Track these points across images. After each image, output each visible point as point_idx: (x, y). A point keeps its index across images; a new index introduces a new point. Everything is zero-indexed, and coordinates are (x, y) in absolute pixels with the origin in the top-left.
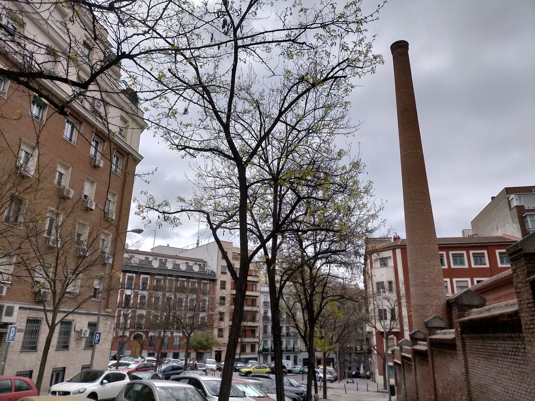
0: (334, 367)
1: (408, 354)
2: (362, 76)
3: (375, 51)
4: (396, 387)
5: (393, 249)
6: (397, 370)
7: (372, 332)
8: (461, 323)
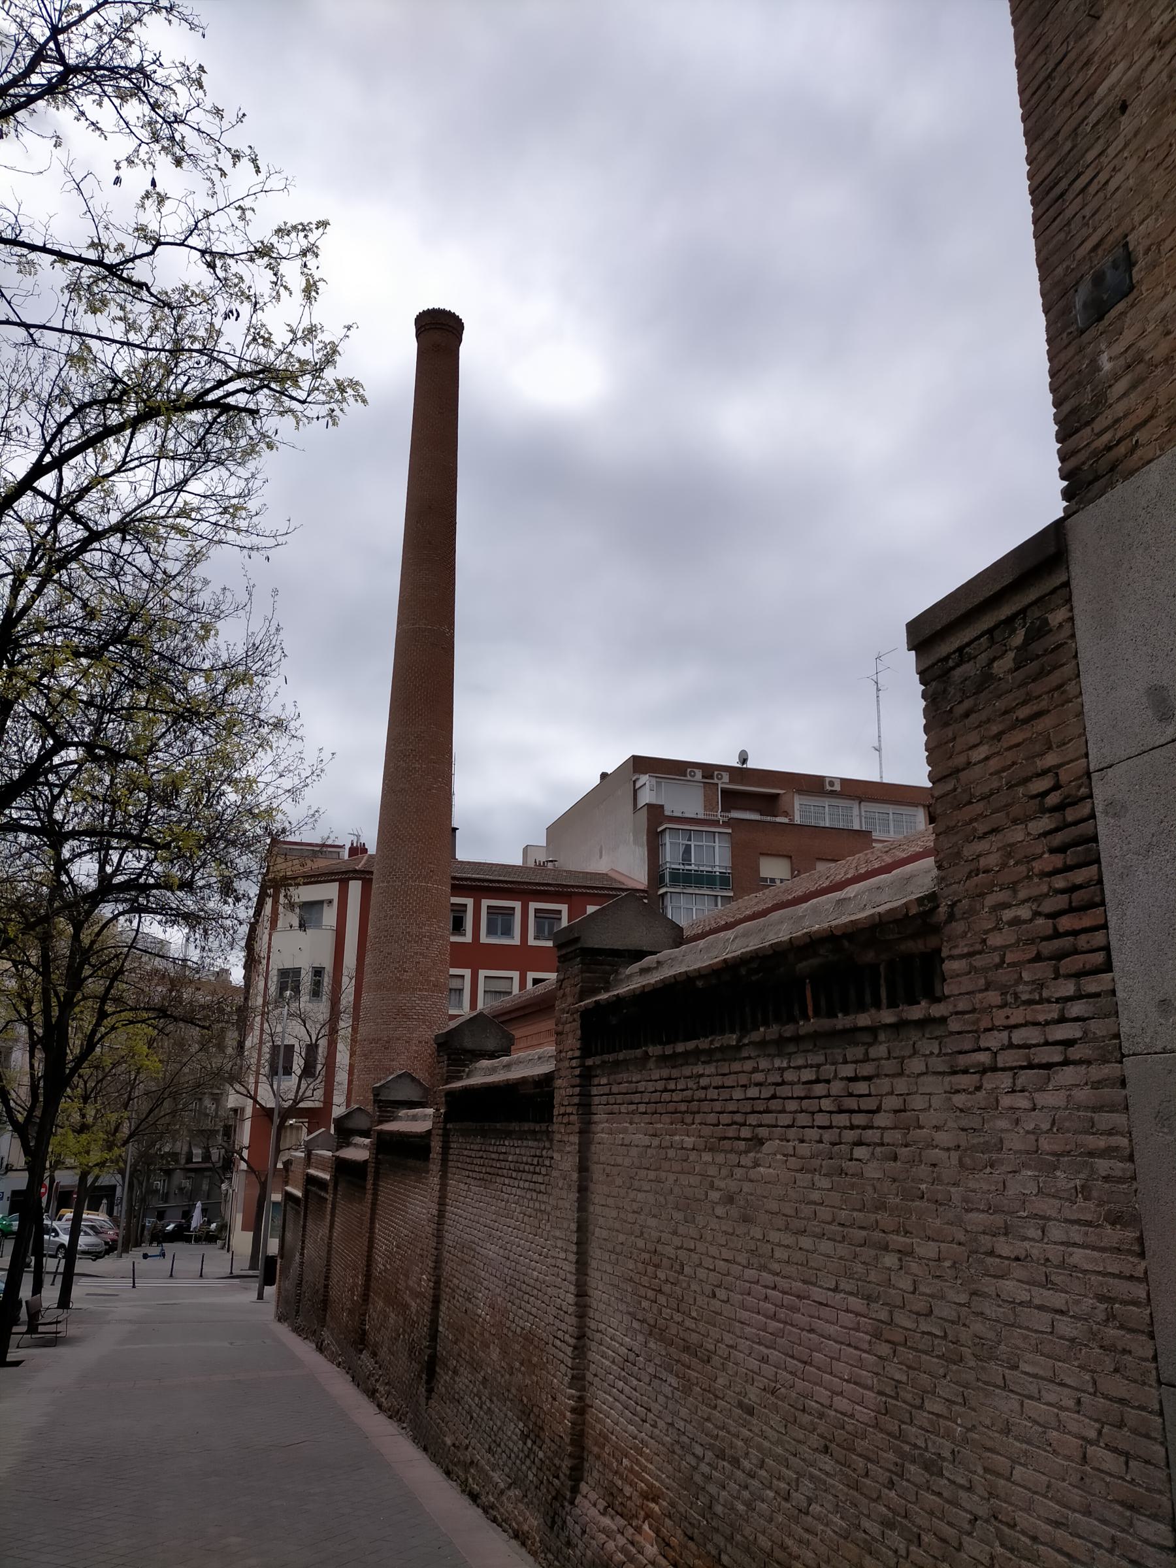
0: (110, 1213)
1: (323, 1170)
4: (279, 1261)
5: (342, 878)
6: (290, 1215)
7: (243, 1109)
8: (450, 1094)
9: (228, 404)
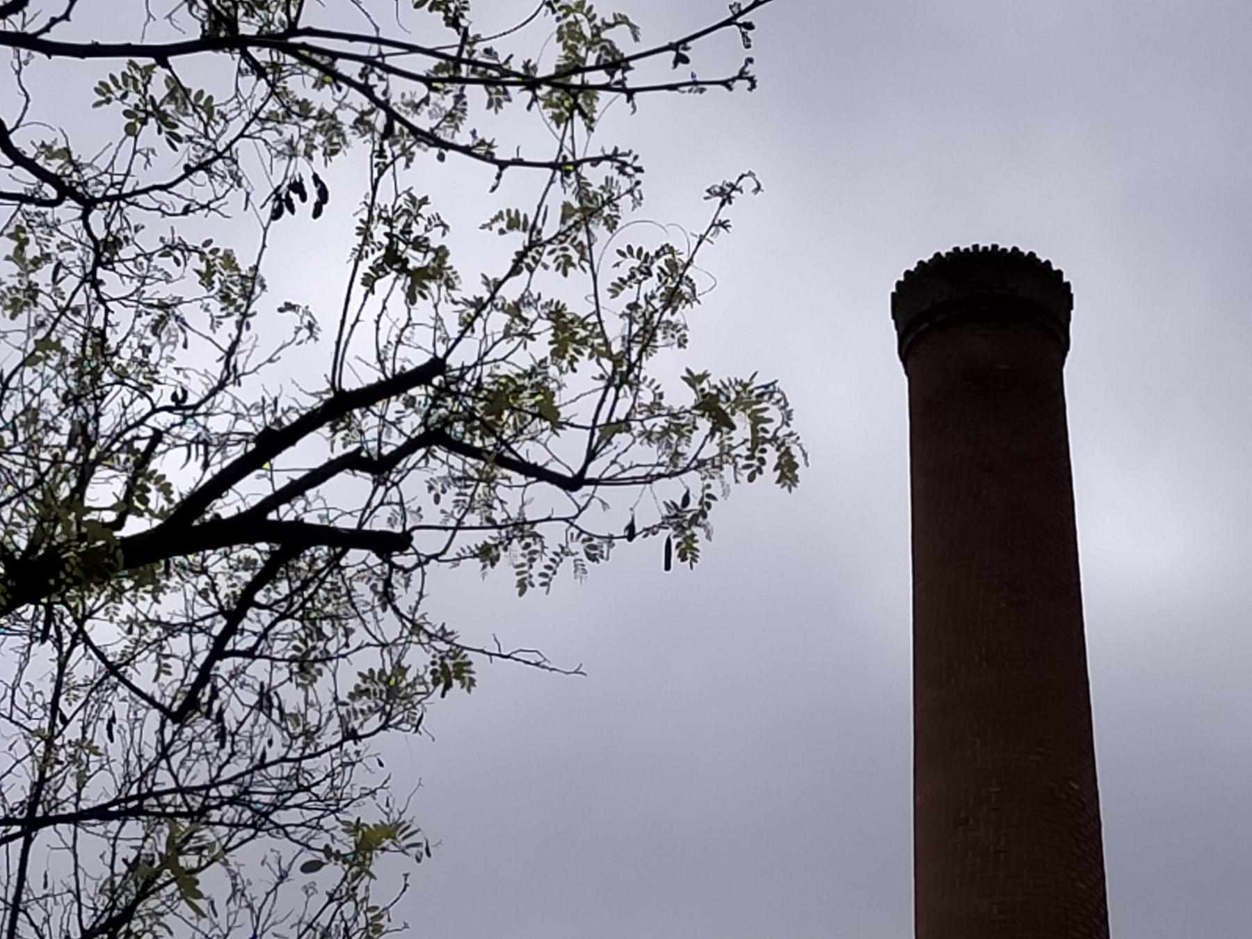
2: (370, 814)
3: (714, 342)
9: (298, 523)
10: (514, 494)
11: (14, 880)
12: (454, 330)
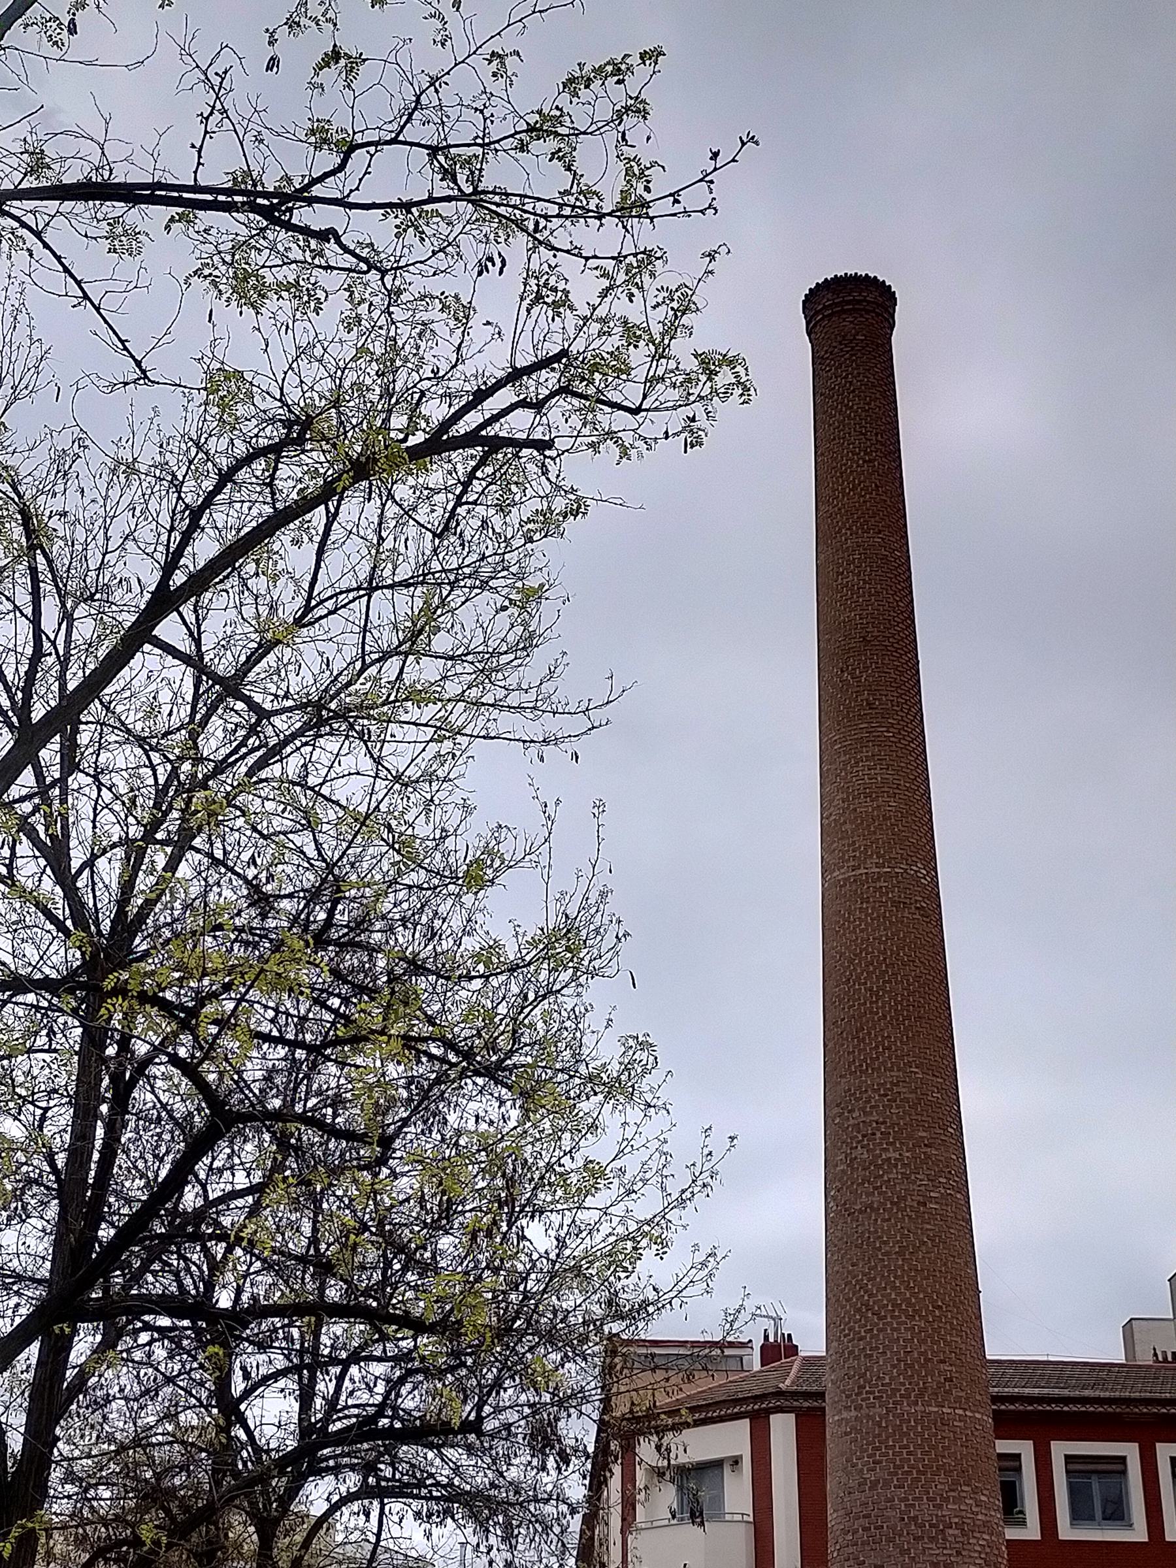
3: (705, 333)
9: (496, 436)
10: (607, 418)
11: (364, 617)
12: (571, 332)
